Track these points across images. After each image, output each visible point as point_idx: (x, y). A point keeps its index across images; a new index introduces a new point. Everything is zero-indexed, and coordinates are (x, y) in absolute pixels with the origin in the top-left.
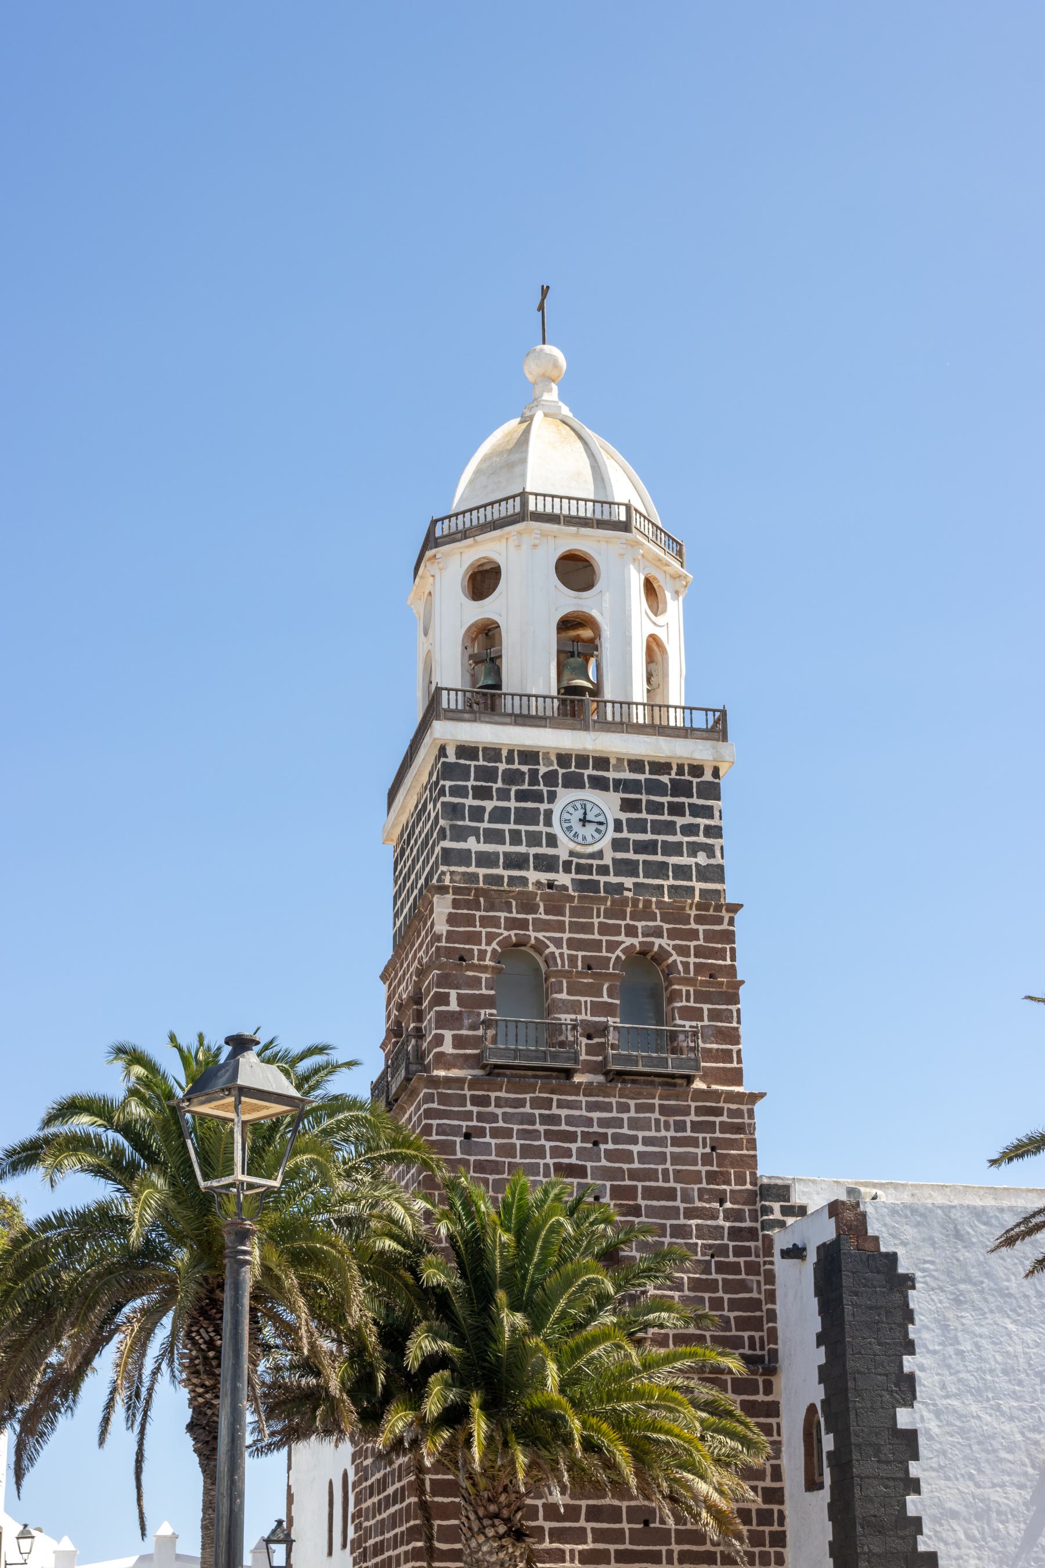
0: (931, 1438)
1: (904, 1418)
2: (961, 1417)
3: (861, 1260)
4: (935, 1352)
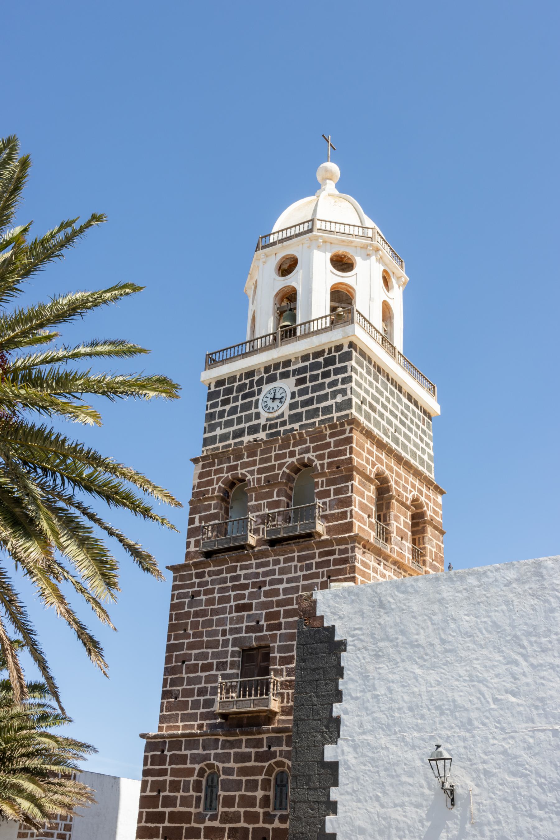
0: (348, 768)
1: (330, 753)
2: (373, 748)
3: (310, 635)
4: (357, 698)
